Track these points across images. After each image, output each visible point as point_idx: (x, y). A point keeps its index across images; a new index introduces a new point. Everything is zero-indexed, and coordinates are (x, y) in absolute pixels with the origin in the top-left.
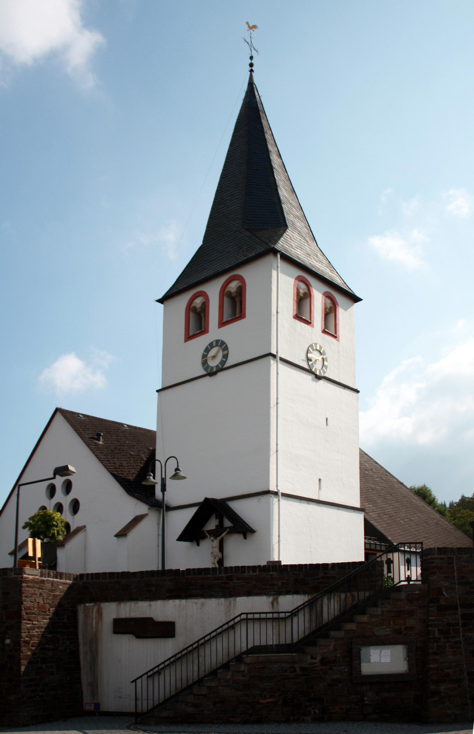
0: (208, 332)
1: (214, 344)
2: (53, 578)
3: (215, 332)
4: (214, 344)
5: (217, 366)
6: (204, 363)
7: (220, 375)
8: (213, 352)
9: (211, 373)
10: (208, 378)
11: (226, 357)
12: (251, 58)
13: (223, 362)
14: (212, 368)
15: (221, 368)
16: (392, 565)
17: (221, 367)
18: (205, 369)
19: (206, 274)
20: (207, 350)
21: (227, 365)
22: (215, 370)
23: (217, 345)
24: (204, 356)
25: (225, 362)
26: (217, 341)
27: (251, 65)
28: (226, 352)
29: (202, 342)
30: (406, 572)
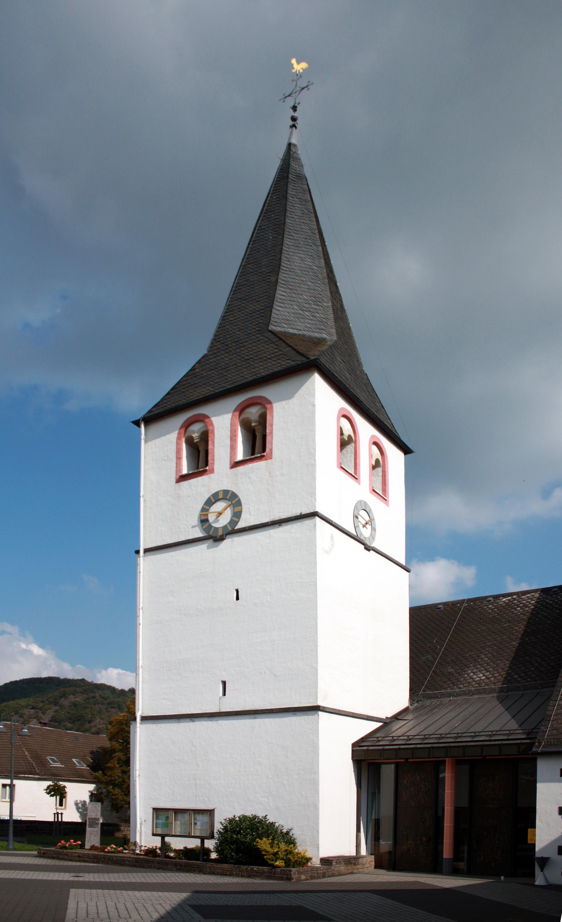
0: (213, 473)
1: (221, 496)
2: (456, 872)
3: (220, 477)
4: (221, 496)
5: (225, 527)
6: (204, 521)
7: (228, 542)
8: (219, 506)
9: (215, 537)
10: (202, 547)
11: (237, 515)
12: (294, 108)
13: (233, 522)
14: (216, 529)
15: (232, 531)
16: (487, 757)
17: (230, 529)
18: (205, 530)
19: (207, 391)
20: (210, 503)
21: (240, 525)
22: (220, 533)
23: (224, 499)
24: (205, 510)
25: (237, 523)
26: (226, 492)
27: (294, 119)
28: (237, 509)
29: (204, 486)
30: (237, 819)
